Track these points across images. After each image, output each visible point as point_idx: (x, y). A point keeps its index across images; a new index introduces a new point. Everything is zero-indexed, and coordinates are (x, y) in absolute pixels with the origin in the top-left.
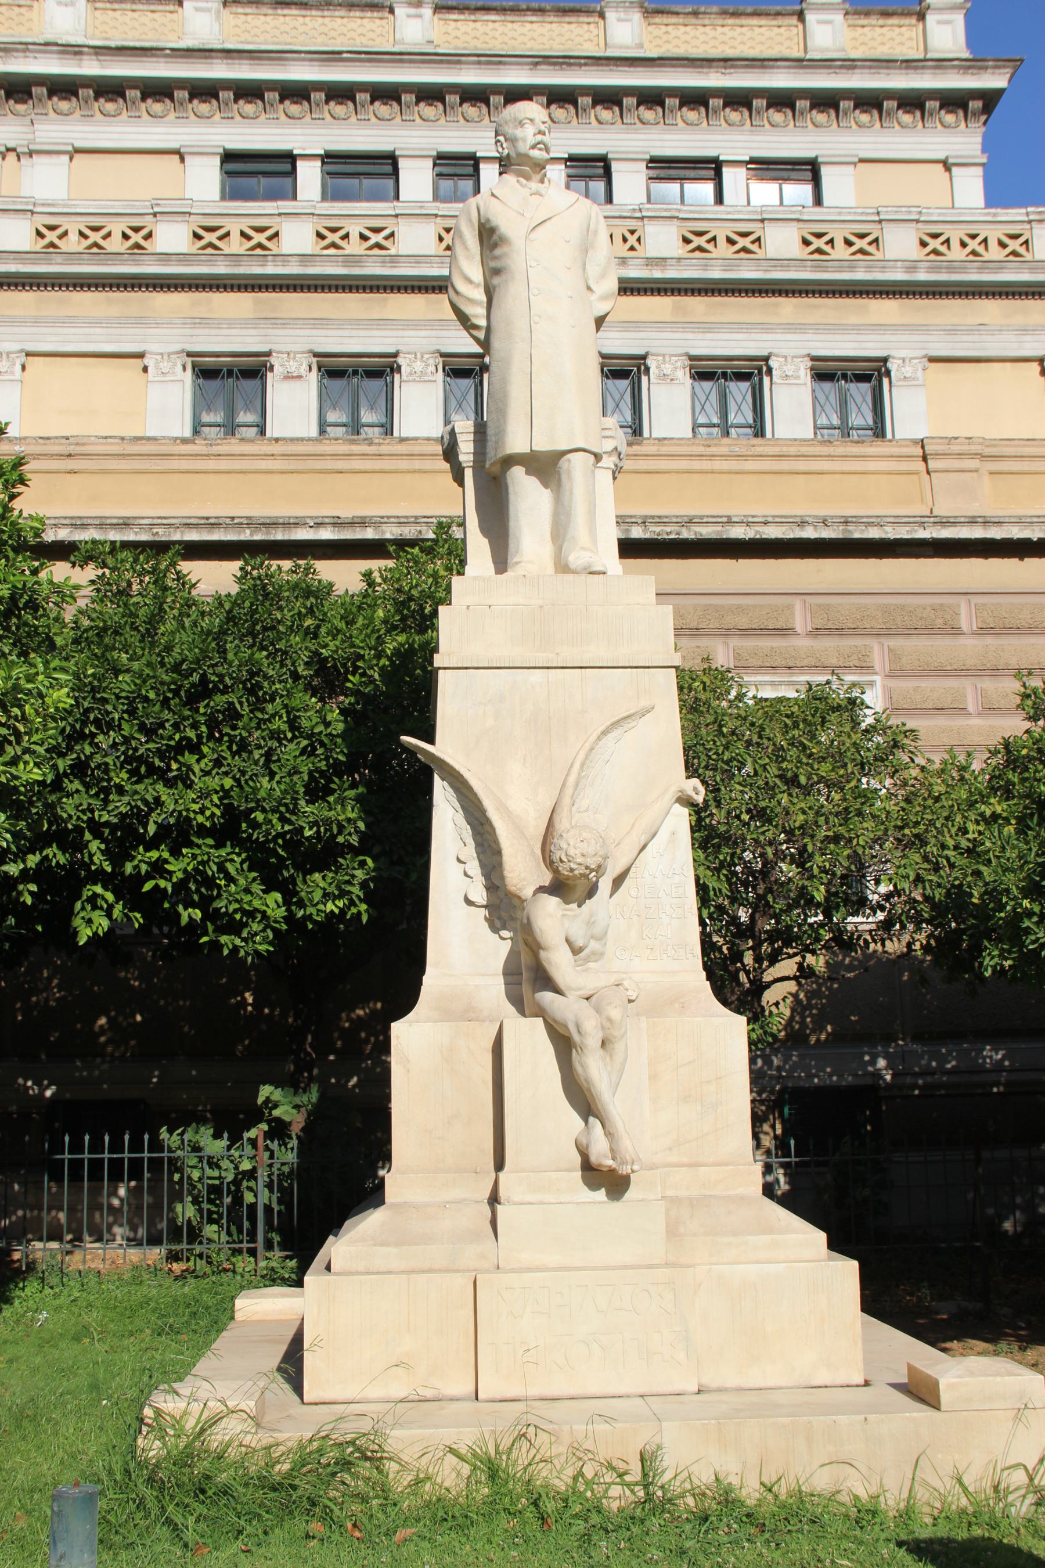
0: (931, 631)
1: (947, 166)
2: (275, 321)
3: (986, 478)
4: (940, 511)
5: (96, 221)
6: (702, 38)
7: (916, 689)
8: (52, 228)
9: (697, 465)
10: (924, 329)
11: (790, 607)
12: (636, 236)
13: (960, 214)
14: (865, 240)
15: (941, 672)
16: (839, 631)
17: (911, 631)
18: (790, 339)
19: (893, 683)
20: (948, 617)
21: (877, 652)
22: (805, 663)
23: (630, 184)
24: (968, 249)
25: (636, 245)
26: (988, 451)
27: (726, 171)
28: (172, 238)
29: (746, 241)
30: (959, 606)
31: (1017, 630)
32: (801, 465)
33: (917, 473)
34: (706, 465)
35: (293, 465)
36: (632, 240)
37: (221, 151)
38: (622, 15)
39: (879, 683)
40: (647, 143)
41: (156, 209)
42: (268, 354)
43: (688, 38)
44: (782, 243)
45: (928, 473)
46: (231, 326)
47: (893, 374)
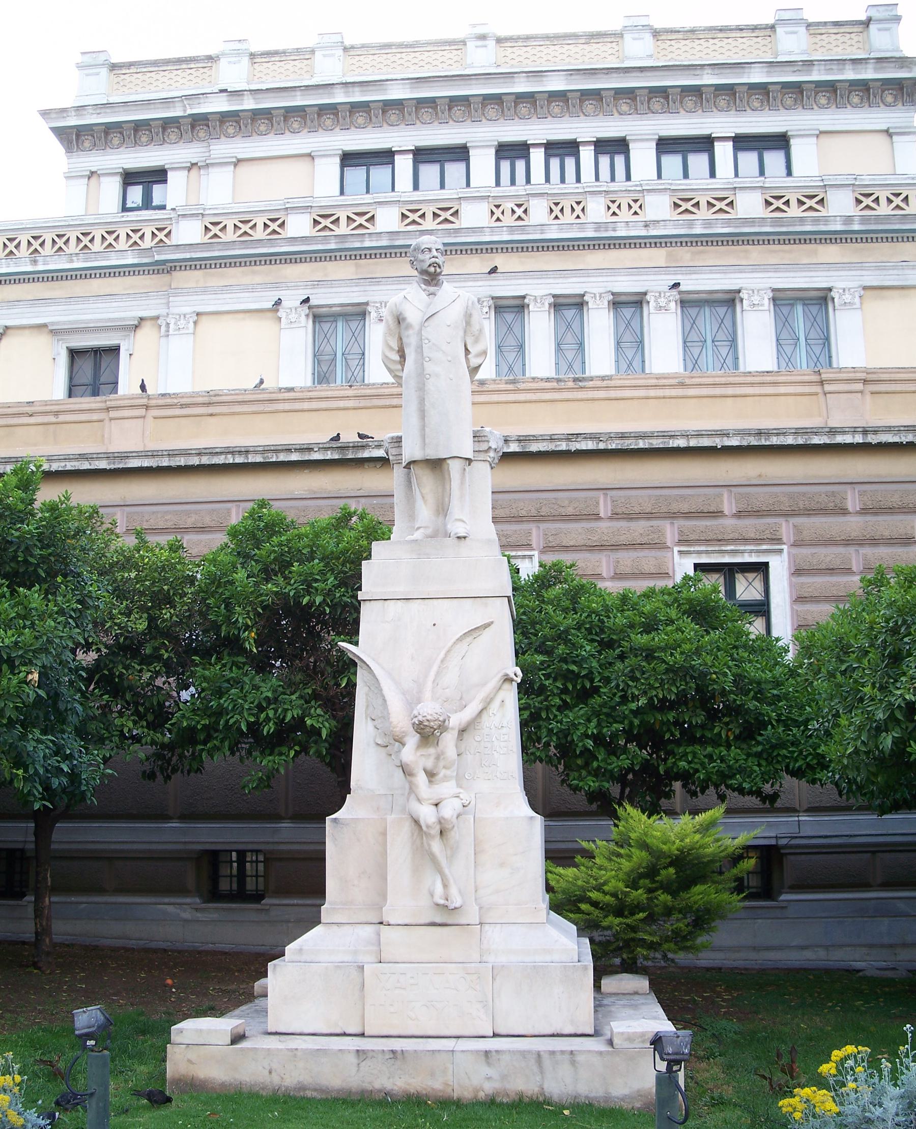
0: (823, 511)
1: (888, 133)
2: (374, 280)
3: (868, 397)
4: (833, 423)
5: (246, 217)
6: (699, 48)
7: (813, 555)
8: (215, 224)
9: (652, 393)
10: (859, 266)
11: (720, 496)
12: (638, 204)
13: (886, 179)
14: (814, 199)
15: (831, 542)
16: (758, 513)
17: (809, 512)
18: (756, 279)
19: (795, 550)
20: (838, 501)
21: (786, 529)
22: (731, 536)
23: (643, 157)
24: (893, 205)
25: (638, 211)
26: (870, 377)
27: (717, 145)
28: (299, 225)
29: (724, 202)
30: (846, 492)
31: (891, 510)
32: (730, 391)
33: (816, 394)
34: (660, 393)
35: (363, 403)
36: (635, 207)
37: (340, 152)
38: (636, 36)
39: (785, 551)
40: (655, 127)
41: (287, 206)
42: (367, 304)
43: (687, 48)
44: (750, 206)
45: (825, 394)
46: (338, 287)
47: (836, 300)
